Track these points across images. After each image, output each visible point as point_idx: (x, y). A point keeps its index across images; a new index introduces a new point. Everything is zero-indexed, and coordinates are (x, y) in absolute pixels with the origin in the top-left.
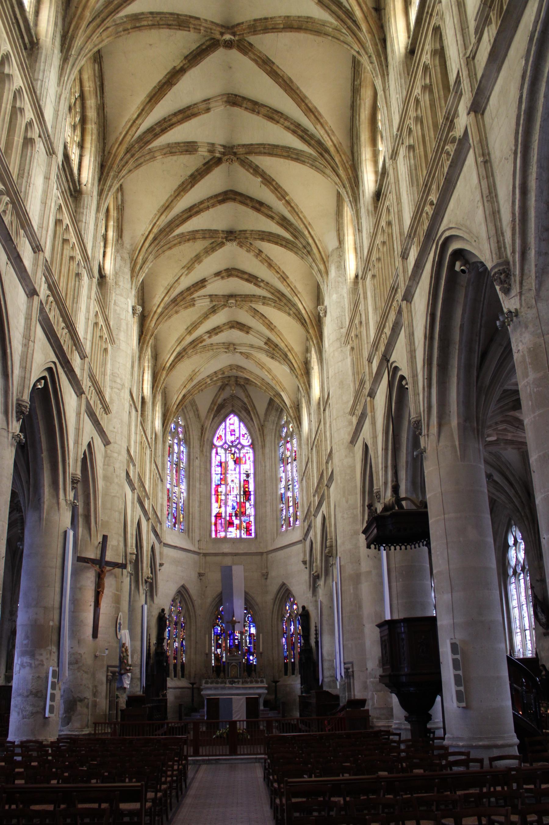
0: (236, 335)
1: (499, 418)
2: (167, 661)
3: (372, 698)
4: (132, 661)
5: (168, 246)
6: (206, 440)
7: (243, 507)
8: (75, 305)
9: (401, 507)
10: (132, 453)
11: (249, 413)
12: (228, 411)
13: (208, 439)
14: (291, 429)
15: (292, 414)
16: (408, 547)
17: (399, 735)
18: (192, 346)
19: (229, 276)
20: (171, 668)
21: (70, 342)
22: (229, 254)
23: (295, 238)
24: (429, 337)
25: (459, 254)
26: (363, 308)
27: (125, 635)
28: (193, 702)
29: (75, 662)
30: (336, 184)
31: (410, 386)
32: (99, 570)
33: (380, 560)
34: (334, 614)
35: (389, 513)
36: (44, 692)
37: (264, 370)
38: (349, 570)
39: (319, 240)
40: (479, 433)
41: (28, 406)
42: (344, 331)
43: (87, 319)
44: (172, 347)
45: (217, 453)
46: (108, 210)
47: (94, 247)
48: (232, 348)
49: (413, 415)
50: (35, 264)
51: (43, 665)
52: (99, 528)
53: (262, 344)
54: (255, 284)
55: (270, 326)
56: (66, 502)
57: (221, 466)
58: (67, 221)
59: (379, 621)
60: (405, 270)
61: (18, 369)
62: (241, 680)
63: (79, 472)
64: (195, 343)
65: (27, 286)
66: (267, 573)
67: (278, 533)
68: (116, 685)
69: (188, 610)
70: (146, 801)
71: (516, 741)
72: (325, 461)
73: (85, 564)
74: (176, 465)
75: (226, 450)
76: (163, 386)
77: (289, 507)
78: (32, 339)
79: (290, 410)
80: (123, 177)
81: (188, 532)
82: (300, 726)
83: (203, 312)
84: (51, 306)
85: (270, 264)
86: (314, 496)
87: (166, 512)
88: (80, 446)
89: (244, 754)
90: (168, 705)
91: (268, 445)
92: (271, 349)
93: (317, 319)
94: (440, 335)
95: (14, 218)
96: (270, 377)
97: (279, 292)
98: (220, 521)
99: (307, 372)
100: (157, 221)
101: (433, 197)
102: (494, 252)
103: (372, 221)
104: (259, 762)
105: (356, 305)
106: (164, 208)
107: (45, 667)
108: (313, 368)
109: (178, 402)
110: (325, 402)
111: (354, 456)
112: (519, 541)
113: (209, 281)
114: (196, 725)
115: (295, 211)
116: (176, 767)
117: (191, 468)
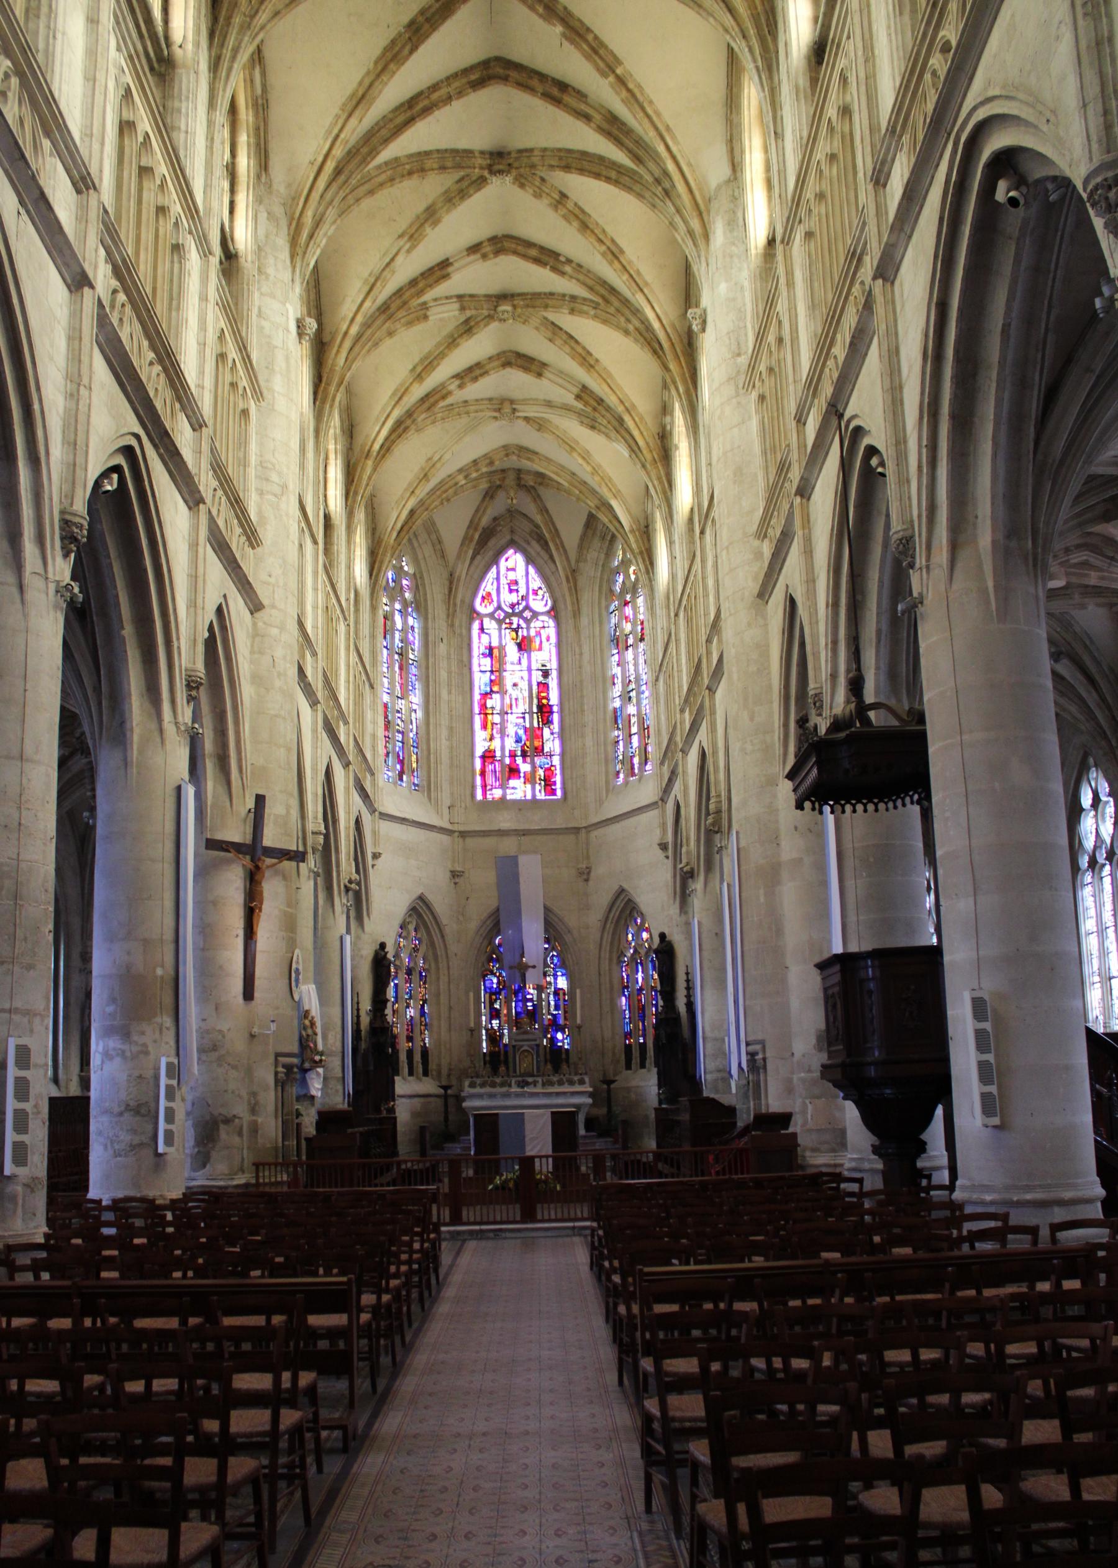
0: (516, 381)
1: (1073, 539)
2: (394, 1046)
3: (804, 1112)
4: (325, 1044)
5: (367, 187)
6: (458, 602)
7: (537, 737)
8: (174, 314)
9: (866, 721)
10: (309, 630)
11: (545, 545)
12: (504, 541)
13: (462, 601)
14: (633, 577)
15: (634, 546)
16: (881, 806)
17: (860, 1181)
18: (426, 405)
19: (497, 253)
20: (403, 1057)
21: (168, 394)
22: (497, 204)
23: (637, 161)
24: (934, 356)
25: (1007, 162)
26: (786, 306)
27: (309, 994)
28: (446, 1122)
29: (211, 1048)
30: (726, 31)
31: (890, 470)
32: (250, 865)
33: (821, 835)
34: (724, 948)
35: (842, 735)
36: (153, 1105)
37: (575, 455)
38: (757, 856)
39: (690, 165)
40: (1038, 566)
41: (86, 524)
42: (743, 360)
43: (202, 345)
44: (383, 409)
45: (482, 629)
46: (233, 109)
47: (207, 187)
48: (507, 409)
49: (896, 526)
50: (82, 217)
51: (147, 1053)
52: (248, 782)
53: (570, 399)
54: (554, 269)
55: (586, 359)
56: (178, 728)
57: (491, 655)
58: (145, 125)
59: (818, 959)
60: (880, 211)
61: (59, 446)
62: (540, 1079)
63: (200, 666)
64: (432, 400)
65: (67, 265)
66: (589, 868)
67: (610, 788)
68: (294, 1090)
69: (432, 944)
70: (360, 1310)
71: (1100, 1192)
72: (704, 638)
73: (222, 854)
74: (400, 654)
75: (500, 622)
76: (368, 493)
77: (630, 736)
78: (85, 381)
79: (630, 536)
80: (262, 28)
81: (427, 789)
82: (660, 1166)
83: (445, 333)
84: (122, 313)
85: (584, 224)
86: (682, 711)
87: (382, 751)
88: (200, 612)
89: (550, 1220)
90: (399, 1128)
91: (585, 609)
92: (589, 409)
93: (685, 341)
94: (957, 351)
95: (27, 111)
96: (589, 469)
97: (604, 283)
98: (491, 767)
99: (666, 455)
100: (341, 130)
101: (951, 33)
102: (1094, 138)
103: (806, 110)
104: (580, 1235)
105: (770, 301)
106: (354, 102)
107: (152, 1057)
108: (677, 448)
109: (399, 525)
110: (703, 516)
111: (766, 625)
112: (1104, 798)
113: (456, 265)
114: (455, 1165)
115: (637, 100)
116: (417, 1246)
117: (431, 660)
